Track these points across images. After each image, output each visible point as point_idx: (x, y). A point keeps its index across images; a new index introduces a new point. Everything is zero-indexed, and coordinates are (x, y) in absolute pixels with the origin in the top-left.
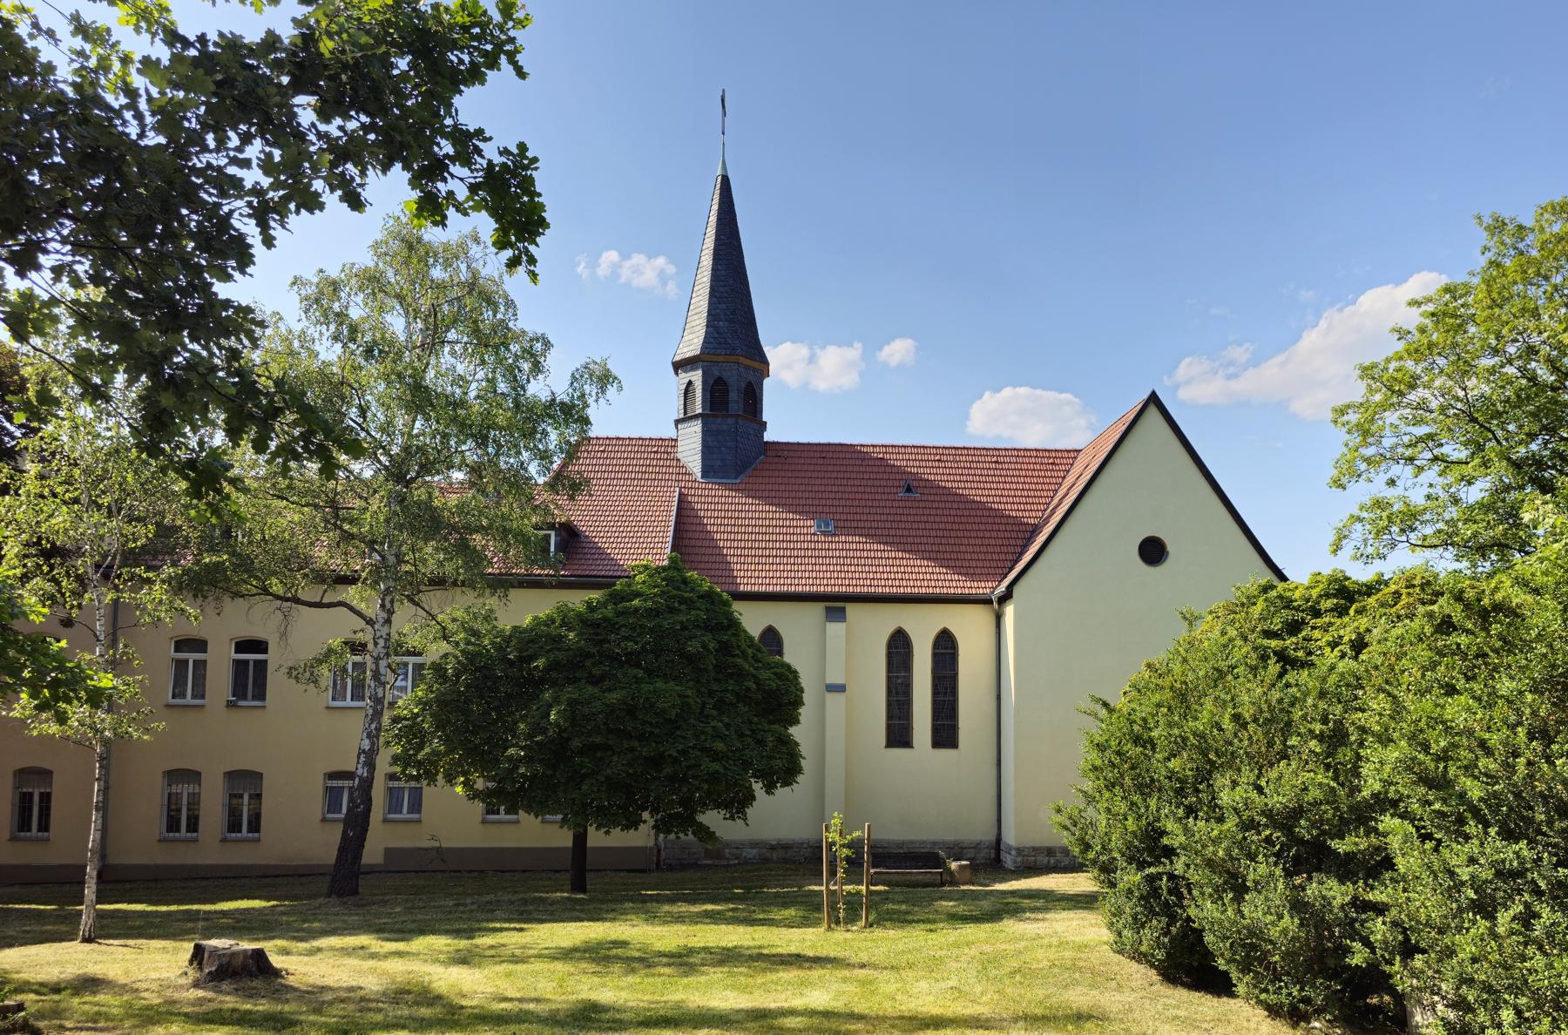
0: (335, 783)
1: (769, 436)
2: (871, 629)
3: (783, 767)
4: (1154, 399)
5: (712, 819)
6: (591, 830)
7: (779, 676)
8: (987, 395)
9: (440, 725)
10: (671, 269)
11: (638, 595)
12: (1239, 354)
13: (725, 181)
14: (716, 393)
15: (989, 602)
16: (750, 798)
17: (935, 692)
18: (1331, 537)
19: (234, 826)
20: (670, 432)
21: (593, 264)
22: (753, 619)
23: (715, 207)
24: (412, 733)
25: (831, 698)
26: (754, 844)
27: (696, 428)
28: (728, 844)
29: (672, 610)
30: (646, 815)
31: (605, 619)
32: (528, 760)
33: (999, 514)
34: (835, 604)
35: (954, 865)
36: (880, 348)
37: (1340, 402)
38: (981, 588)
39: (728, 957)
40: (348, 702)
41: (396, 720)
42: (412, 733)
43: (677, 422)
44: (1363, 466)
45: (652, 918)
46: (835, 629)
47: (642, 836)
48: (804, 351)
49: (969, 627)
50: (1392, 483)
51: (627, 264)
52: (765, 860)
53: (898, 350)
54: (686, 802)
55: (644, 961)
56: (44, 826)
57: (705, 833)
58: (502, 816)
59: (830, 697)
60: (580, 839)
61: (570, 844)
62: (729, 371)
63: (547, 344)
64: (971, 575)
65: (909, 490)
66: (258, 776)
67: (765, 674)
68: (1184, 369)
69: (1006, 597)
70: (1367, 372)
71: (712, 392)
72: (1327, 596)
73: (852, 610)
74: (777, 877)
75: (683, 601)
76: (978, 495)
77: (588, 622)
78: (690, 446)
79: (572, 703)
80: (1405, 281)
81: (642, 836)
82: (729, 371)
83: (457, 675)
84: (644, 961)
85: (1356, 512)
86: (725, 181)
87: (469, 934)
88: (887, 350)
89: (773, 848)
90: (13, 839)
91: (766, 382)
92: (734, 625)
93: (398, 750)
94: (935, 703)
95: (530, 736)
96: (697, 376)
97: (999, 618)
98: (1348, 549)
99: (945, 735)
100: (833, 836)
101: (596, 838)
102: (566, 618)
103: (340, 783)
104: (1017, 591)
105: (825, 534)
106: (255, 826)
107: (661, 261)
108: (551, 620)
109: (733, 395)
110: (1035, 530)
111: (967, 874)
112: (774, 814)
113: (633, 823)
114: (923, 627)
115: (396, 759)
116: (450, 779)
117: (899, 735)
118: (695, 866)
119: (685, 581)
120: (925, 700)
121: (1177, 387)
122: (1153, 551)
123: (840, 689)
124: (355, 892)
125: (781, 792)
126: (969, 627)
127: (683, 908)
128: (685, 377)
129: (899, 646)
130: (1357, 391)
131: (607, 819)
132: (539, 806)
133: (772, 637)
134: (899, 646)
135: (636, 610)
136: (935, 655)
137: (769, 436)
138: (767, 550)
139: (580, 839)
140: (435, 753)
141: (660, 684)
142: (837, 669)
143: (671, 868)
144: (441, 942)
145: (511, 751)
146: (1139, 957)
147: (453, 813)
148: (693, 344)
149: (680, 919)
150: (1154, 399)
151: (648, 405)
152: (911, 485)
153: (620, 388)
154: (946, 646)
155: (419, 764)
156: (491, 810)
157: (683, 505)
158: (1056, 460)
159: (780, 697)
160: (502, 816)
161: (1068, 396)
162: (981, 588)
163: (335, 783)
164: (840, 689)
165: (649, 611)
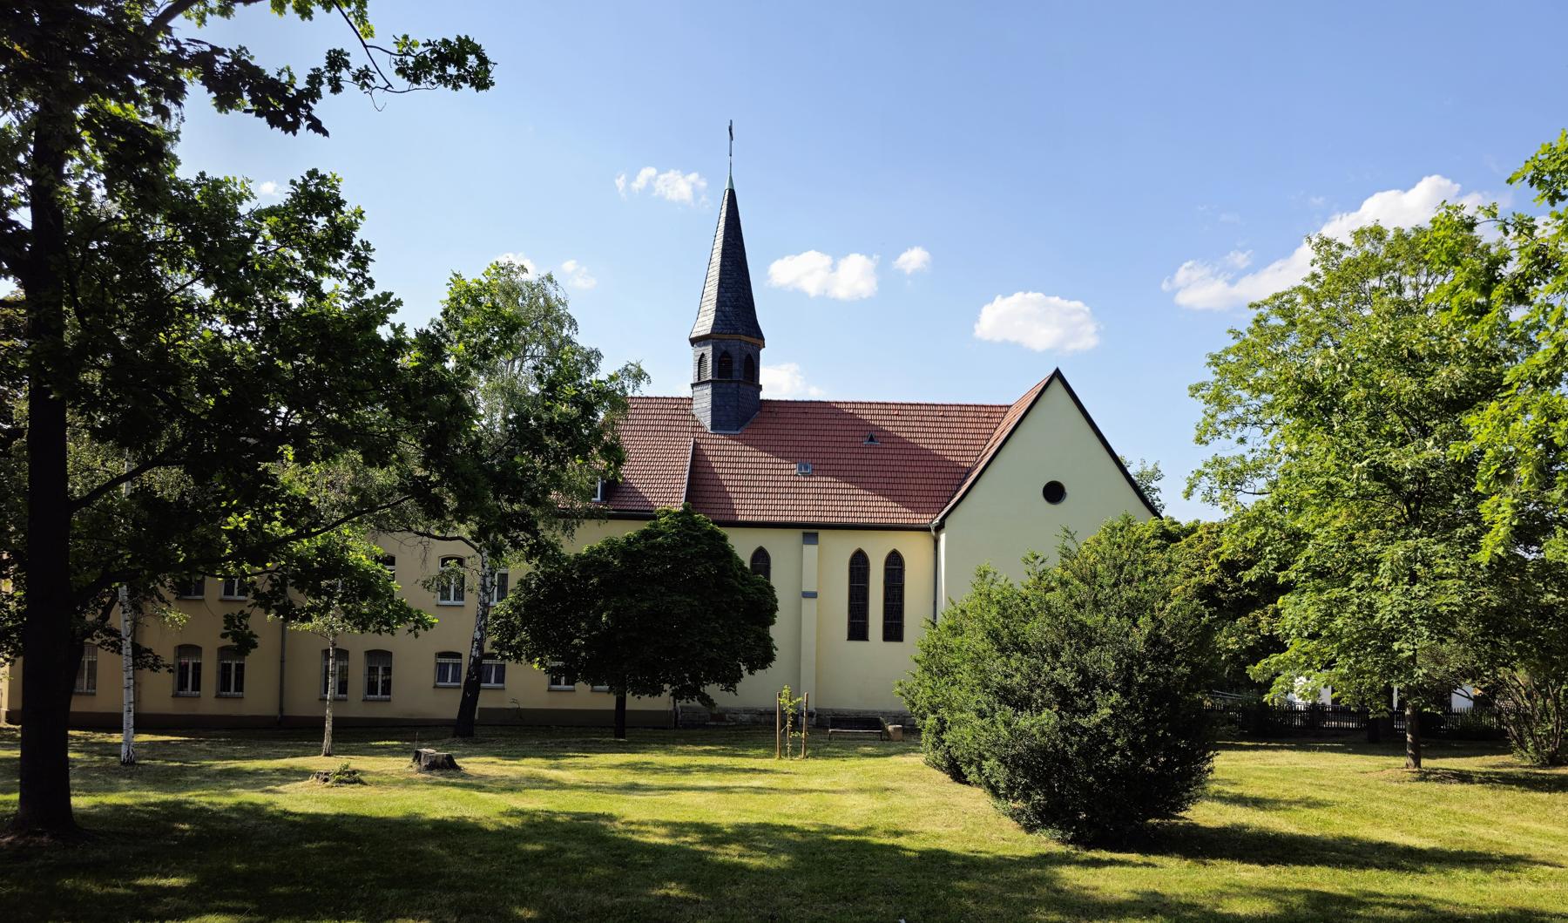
0: (443, 660)
1: (764, 395)
2: (840, 549)
3: (763, 656)
4: (1057, 374)
5: (713, 690)
6: (629, 695)
7: (760, 591)
8: (998, 298)
9: (526, 620)
10: (703, 184)
11: (661, 534)
12: (1240, 260)
13: (732, 194)
14: (723, 364)
15: (928, 530)
16: (739, 677)
17: (886, 599)
18: (1185, 487)
19: (372, 688)
20: (686, 392)
21: (632, 177)
22: (743, 545)
23: (724, 215)
24: (508, 629)
25: (808, 604)
26: (747, 711)
27: (708, 390)
28: (727, 711)
29: (685, 545)
30: (666, 686)
31: (639, 551)
32: (586, 648)
33: (942, 459)
34: (811, 531)
35: (890, 728)
36: (897, 256)
37: (1194, 382)
38: (923, 519)
39: (711, 769)
40: (452, 602)
41: (496, 617)
42: (508, 629)
43: (693, 386)
44: (1221, 427)
45: (670, 752)
46: (810, 550)
47: (662, 702)
48: (827, 260)
49: (913, 549)
50: (1242, 441)
51: (662, 177)
52: (755, 723)
53: (914, 258)
54: (694, 678)
55: (664, 769)
56: (240, 688)
57: (706, 700)
58: (563, 686)
59: (805, 601)
60: (621, 702)
61: (613, 707)
62: (734, 340)
63: (599, 356)
64: (917, 509)
65: (871, 439)
66: (389, 654)
67: (750, 590)
68: (1181, 275)
69: (940, 527)
70: (1215, 360)
71: (720, 362)
72: (1155, 537)
73: (822, 534)
74: (753, 731)
75: (693, 538)
76: (922, 443)
77: (626, 551)
78: (703, 403)
79: (616, 609)
80: (1413, 186)
81: (662, 702)
82: (734, 340)
83: (538, 587)
84: (664, 769)
85: (1201, 467)
86: (732, 194)
87: (556, 758)
88: (904, 257)
89: (761, 714)
90: (175, 696)
91: (762, 352)
92: (728, 554)
93: (496, 638)
94: (886, 607)
95: (588, 632)
96: (708, 351)
97: (936, 542)
98: (1198, 495)
99: (894, 631)
100: (784, 701)
101: (634, 703)
102: (612, 545)
103: (447, 660)
104: (947, 522)
105: (805, 475)
106: (387, 688)
107: (693, 177)
108: (600, 551)
109: (736, 366)
110: (969, 471)
111: (900, 734)
112: (757, 689)
113: (656, 691)
114: (877, 549)
115: (494, 644)
116: (530, 659)
117: (858, 631)
118: (704, 726)
119: (694, 523)
120: (875, 602)
121: (1175, 291)
122: (1054, 492)
123: (814, 595)
124: (471, 734)
125: (758, 672)
126: (913, 549)
127: (691, 748)
128: (700, 350)
129: (859, 564)
130: (1209, 375)
131: (640, 690)
132: (593, 679)
133: (761, 556)
134: (859, 564)
135: (661, 544)
136: (886, 570)
137: (764, 395)
138: (759, 484)
139: (621, 702)
140: (524, 642)
141: (676, 598)
142: (808, 587)
143: (685, 727)
144: (539, 761)
145: (576, 641)
146: (938, 767)
147: (527, 683)
148: (705, 325)
149: (687, 753)
150: (1057, 374)
151: (675, 374)
152: (874, 435)
153: (649, 382)
154: (895, 563)
155: (510, 648)
156: (555, 682)
157: (697, 455)
158: (994, 413)
159: (762, 607)
160: (563, 686)
161: (1078, 304)
162: (923, 519)
163: (443, 660)
164: (814, 595)
165: (670, 547)
